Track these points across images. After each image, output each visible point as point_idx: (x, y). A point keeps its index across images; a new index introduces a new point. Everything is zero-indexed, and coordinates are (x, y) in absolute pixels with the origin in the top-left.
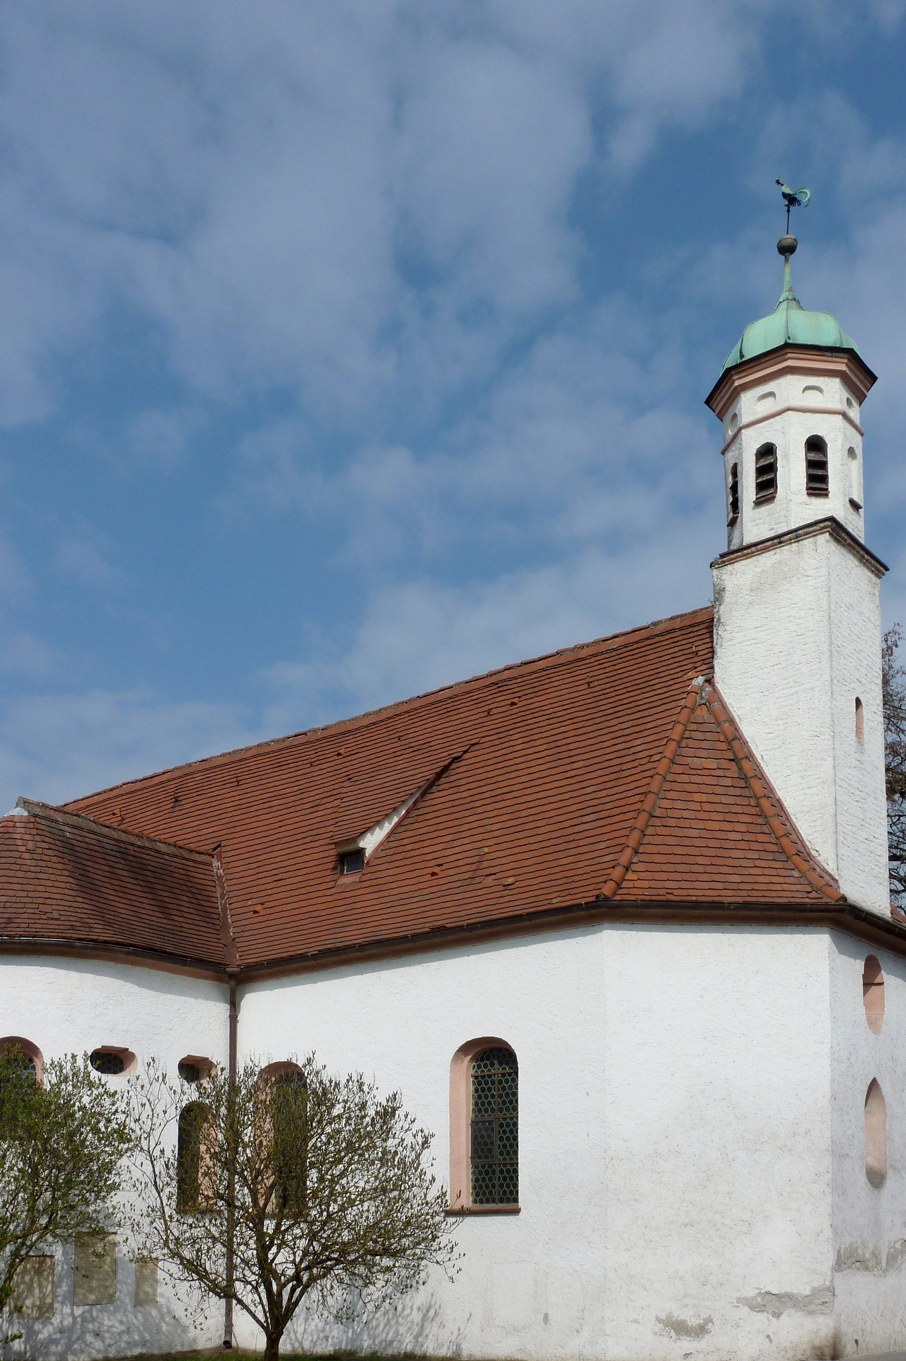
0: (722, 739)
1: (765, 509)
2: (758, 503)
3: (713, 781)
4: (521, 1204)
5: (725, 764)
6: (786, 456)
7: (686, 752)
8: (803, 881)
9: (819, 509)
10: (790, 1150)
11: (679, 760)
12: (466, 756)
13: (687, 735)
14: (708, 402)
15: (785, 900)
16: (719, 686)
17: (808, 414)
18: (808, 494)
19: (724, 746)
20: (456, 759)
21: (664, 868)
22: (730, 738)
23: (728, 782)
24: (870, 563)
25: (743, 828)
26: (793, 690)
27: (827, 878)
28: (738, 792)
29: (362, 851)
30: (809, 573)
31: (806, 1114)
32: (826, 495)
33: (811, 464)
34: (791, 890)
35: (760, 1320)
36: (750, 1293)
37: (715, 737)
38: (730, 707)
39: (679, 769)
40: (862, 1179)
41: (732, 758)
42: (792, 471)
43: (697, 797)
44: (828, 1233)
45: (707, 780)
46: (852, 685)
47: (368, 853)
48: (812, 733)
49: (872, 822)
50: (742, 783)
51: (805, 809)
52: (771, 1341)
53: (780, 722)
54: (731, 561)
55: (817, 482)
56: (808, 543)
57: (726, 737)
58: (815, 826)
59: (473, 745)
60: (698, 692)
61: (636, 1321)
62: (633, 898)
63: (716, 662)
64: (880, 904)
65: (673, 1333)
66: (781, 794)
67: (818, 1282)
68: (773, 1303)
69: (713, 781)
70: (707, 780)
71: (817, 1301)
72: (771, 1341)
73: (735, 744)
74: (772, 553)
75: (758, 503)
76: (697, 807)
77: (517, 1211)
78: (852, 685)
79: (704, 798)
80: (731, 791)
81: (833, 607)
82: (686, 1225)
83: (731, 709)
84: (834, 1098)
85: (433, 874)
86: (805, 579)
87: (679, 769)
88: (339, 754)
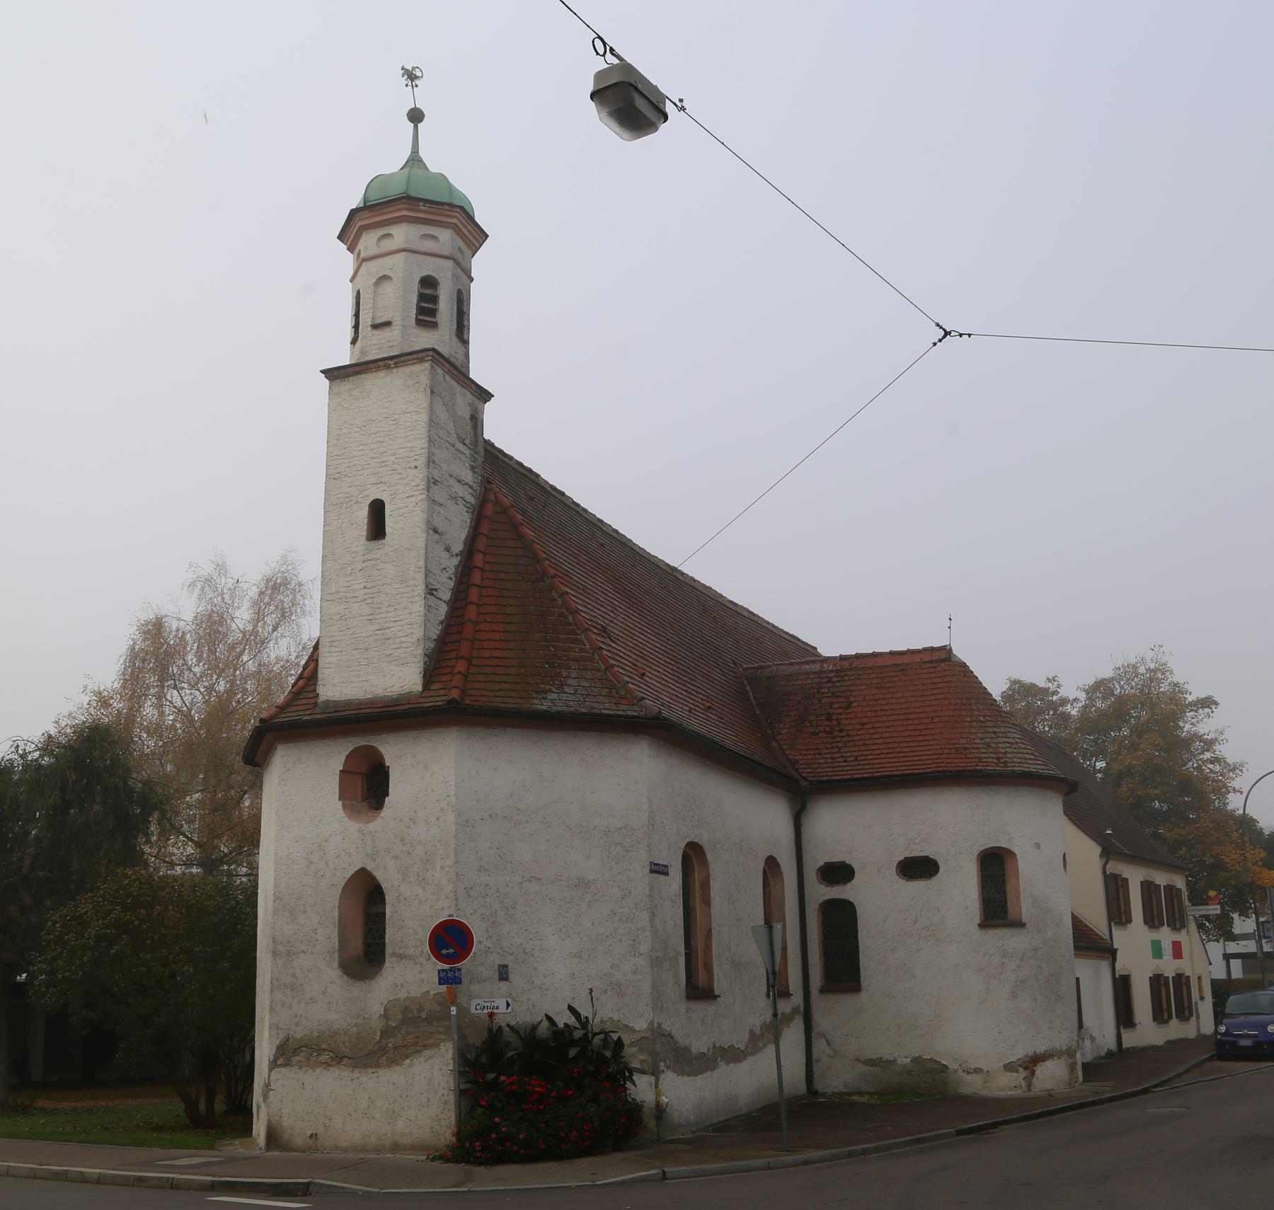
9: (424, 339)
14: (340, 237)
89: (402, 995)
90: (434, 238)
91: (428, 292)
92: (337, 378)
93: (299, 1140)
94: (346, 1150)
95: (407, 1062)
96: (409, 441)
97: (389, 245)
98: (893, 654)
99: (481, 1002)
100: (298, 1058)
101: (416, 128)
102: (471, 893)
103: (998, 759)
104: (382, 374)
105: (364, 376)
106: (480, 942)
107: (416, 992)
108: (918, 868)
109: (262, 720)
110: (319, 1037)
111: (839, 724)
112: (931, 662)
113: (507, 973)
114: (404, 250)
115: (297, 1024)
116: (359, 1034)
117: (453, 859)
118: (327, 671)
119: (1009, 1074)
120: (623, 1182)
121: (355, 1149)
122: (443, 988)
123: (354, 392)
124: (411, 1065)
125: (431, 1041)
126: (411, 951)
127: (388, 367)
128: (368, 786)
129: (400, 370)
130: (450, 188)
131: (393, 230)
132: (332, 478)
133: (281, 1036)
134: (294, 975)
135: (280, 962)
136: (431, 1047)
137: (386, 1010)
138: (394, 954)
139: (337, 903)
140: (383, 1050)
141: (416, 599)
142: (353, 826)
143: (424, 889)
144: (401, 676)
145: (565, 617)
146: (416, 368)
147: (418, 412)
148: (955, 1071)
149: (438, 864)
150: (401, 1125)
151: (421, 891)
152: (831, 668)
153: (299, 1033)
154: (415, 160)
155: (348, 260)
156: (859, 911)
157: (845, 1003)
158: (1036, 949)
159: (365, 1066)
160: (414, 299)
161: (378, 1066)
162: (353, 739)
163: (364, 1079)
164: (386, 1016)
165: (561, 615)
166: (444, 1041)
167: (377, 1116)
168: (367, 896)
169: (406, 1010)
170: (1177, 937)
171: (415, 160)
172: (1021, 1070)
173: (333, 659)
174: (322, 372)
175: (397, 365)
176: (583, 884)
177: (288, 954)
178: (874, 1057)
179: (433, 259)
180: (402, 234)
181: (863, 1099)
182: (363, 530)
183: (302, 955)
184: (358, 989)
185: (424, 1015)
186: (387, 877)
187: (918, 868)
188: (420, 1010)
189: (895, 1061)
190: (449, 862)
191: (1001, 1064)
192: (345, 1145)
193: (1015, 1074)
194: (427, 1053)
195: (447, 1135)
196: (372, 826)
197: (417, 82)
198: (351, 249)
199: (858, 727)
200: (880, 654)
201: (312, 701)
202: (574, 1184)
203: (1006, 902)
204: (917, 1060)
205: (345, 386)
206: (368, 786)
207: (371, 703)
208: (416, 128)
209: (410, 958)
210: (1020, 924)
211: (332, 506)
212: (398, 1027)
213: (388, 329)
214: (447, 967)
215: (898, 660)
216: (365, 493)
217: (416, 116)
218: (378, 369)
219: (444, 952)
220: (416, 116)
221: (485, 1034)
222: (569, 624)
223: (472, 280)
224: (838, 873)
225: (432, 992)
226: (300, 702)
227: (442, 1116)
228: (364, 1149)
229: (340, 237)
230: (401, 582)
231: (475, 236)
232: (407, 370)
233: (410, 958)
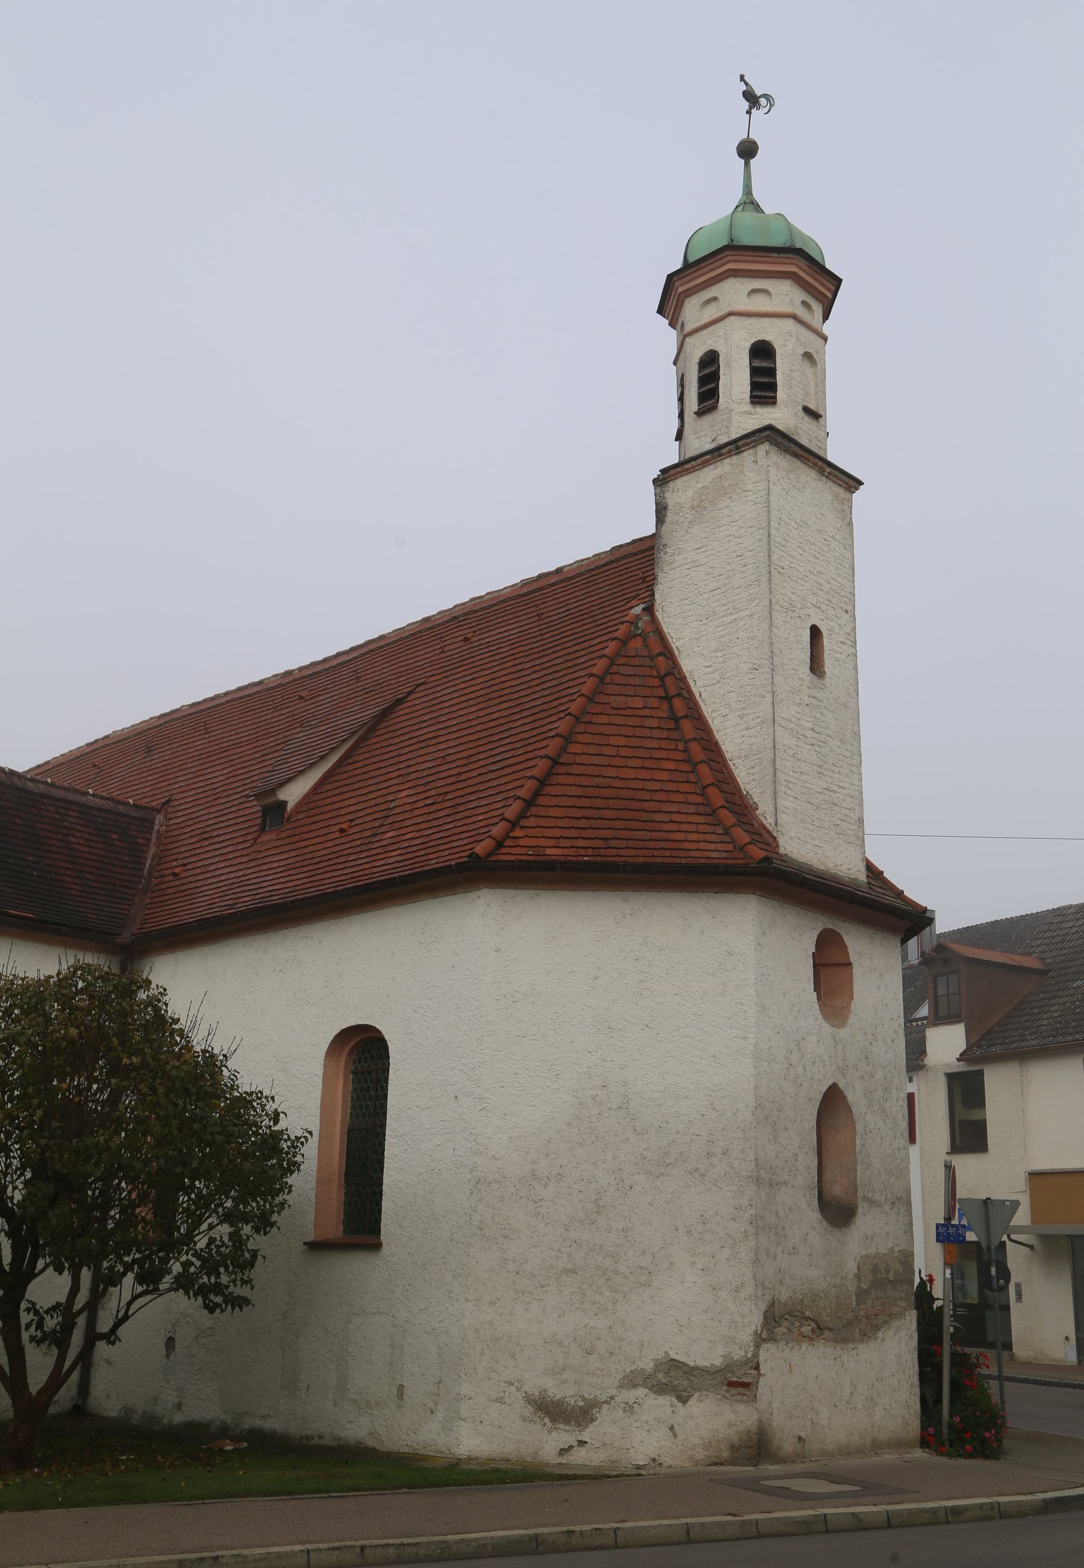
0: (655, 673)
1: (708, 419)
2: (700, 414)
3: (637, 722)
4: (383, 1238)
5: (655, 703)
6: (728, 363)
7: (610, 689)
8: (726, 839)
9: (765, 416)
10: (703, 1176)
11: (601, 698)
12: (411, 697)
13: (614, 669)
14: (661, 311)
15: (641, 860)
16: (659, 615)
17: (766, 320)
18: (752, 403)
19: (657, 682)
20: (399, 701)
21: (560, 823)
22: (663, 672)
23: (655, 723)
24: (835, 476)
25: (665, 776)
26: (732, 618)
27: (766, 835)
28: (665, 734)
29: (284, 803)
30: (749, 487)
31: (723, 1129)
32: (775, 403)
33: (754, 371)
34: (712, 849)
35: (658, 1407)
36: (648, 1365)
37: (647, 671)
38: (669, 638)
39: (599, 709)
40: (812, 1215)
41: (663, 695)
42: (735, 380)
43: (613, 741)
44: (750, 1289)
45: (630, 721)
46: (806, 611)
47: (289, 807)
48: (750, 665)
49: (834, 769)
50: (672, 725)
51: (743, 754)
52: (675, 1435)
53: (719, 654)
54: (675, 477)
55: (763, 388)
56: (748, 455)
57: (659, 672)
58: (753, 774)
59: (419, 685)
60: (634, 622)
61: (500, 1400)
62: (513, 858)
63: (656, 589)
64: (851, 866)
65: (547, 1420)
66: (719, 736)
67: (738, 1354)
68: (675, 1379)
69: (637, 722)
70: (630, 721)
71: (738, 1381)
72: (675, 1435)
73: (669, 681)
74: (712, 467)
75: (700, 414)
76: (613, 751)
77: (377, 1246)
78: (806, 611)
79: (623, 741)
80: (656, 733)
81: (774, 524)
82: (567, 1271)
83: (670, 640)
84: (759, 1106)
85: (342, 831)
86: (745, 494)
87: (599, 709)
88: (301, 698)
91: (764, 364)
93: (789, 1446)
101: (747, 164)
104: (813, 474)
110: (802, 1301)
125: (895, 1309)
127: (821, 472)
129: (829, 483)
130: (790, 229)
133: (768, 1298)
137: (858, 1267)
153: (784, 1295)
154: (749, 203)
155: (670, 337)
164: (858, 1277)
167: (859, 1406)
170: (911, 1088)
171: (749, 203)
186: (854, 1096)
194: (895, 1324)
198: (672, 324)
207: (811, 870)
208: (747, 164)
217: (748, 150)
220: (748, 150)
223: (825, 339)
225: (897, 1249)
229: (661, 311)
231: (821, 284)
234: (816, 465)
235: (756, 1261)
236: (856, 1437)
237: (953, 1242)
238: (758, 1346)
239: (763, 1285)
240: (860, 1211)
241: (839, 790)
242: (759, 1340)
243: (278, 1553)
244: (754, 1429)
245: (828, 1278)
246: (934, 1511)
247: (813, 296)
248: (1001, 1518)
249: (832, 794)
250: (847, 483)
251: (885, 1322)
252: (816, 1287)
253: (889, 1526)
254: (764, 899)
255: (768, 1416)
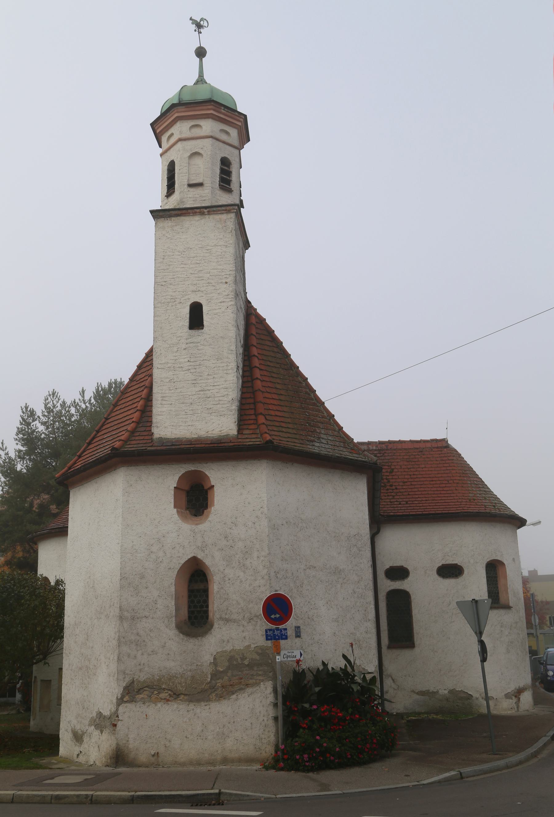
14: (152, 125)
89: (229, 648)
90: (227, 133)
92: (161, 217)
93: (143, 758)
94: (183, 764)
95: (234, 696)
96: (220, 265)
97: (197, 132)
98: (411, 442)
99: (286, 652)
100: (141, 696)
101: (201, 61)
102: (278, 575)
103: (494, 506)
104: (197, 218)
105: (182, 218)
106: (69, 616)
107: (239, 646)
108: (450, 571)
109: (113, 449)
110: (159, 680)
111: (389, 482)
112: (438, 448)
113: (300, 632)
114: (211, 137)
115: (140, 670)
116: (193, 677)
117: (267, 552)
118: (160, 418)
119: (508, 700)
120: (439, 782)
121: (191, 763)
122: (269, 643)
123: (175, 228)
124: (237, 700)
125: (251, 681)
126: (235, 616)
127: (202, 214)
128: (195, 499)
129: (211, 216)
131: (202, 122)
132: (160, 285)
133: (128, 679)
134: (138, 634)
135: (126, 625)
136: (253, 685)
138: (221, 618)
139: (173, 581)
140: (213, 688)
141: (230, 371)
142: (186, 527)
143: (244, 572)
144: (221, 423)
145: (309, 394)
146: (224, 216)
147: (226, 247)
148: (477, 699)
149: (255, 554)
150: (229, 743)
151: (242, 574)
152: (374, 448)
153: (142, 677)
154: (201, 80)
156: (413, 597)
157: (405, 655)
158: (516, 623)
159: (199, 701)
160: (218, 171)
161: (209, 700)
162: (184, 466)
163: (198, 711)
164: (215, 663)
165: (306, 393)
166: (263, 681)
167: (209, 737)
168: (195, 579)
169: (231, 659)
171: (201, 80)
172: (514, 697)
173: (164, 409)
174: (152, 212)
175: (209, 213)
176: (337, 571)
177: (133, 618)
178: (424, 689)
179: (227, 147)
180: (208, 126)
181: (439, 717)
182: (186, 322)
183: (144, 620)
184: (191, 644)
185: (246, 662)
186: (214, 563)
187: (450, 571)
188: (243, 658)
189: (438, 692)
190: (263, 553)
191: (503, 694)
192: (182, 760)
193: (511, 700)
194: (249, 690)
195: (268, 751)
196: (202, 527)
197: (202, 30)
199: (401, 484)
200: (404, 442)
201: (150, 437)
202: (411, 784)
203: (498, 593)
204: (452, 692)
205: (168, 223)
206: (195, 499)
207: (199, 440)
208: (201, 61)
209: (235, 621)
210: (507, 607)
211: (160, 303)
212: (225, 672)
213: (200, 188)
214: (274, 627)
215: (417, 446)
216: (187, 297)
217: (201, 53)
218: (195, 214)
219: (273, 616)
220: (201, 53)
221: (291, 676)
222: (312, 399)
224: (399, 573)
225: (253, 646)
226: (133, 438)
227: (263, 736)
228: (199, 763)
230: (218, 359)
232: (217, 217)
233: (235, 621)
234: (196, 213)
235: (119, 659)
236: (206, 755)
237: (271, 639)
238: (118, 705)
239: (124, 673)
240: (216, 626)
241: (214, 388)
242: (120, 701)
243: (58, 795)
244: (115, 748)
245: (184, 666)
246: (44, 796)
247: (167, 130)
248: (91, 803)
249: (208, 392)
250: (226, 210)
251: (241, 689)
252: (173, 672)
253: (12, 802)
254: (130, 468)
255: (124, 742)
